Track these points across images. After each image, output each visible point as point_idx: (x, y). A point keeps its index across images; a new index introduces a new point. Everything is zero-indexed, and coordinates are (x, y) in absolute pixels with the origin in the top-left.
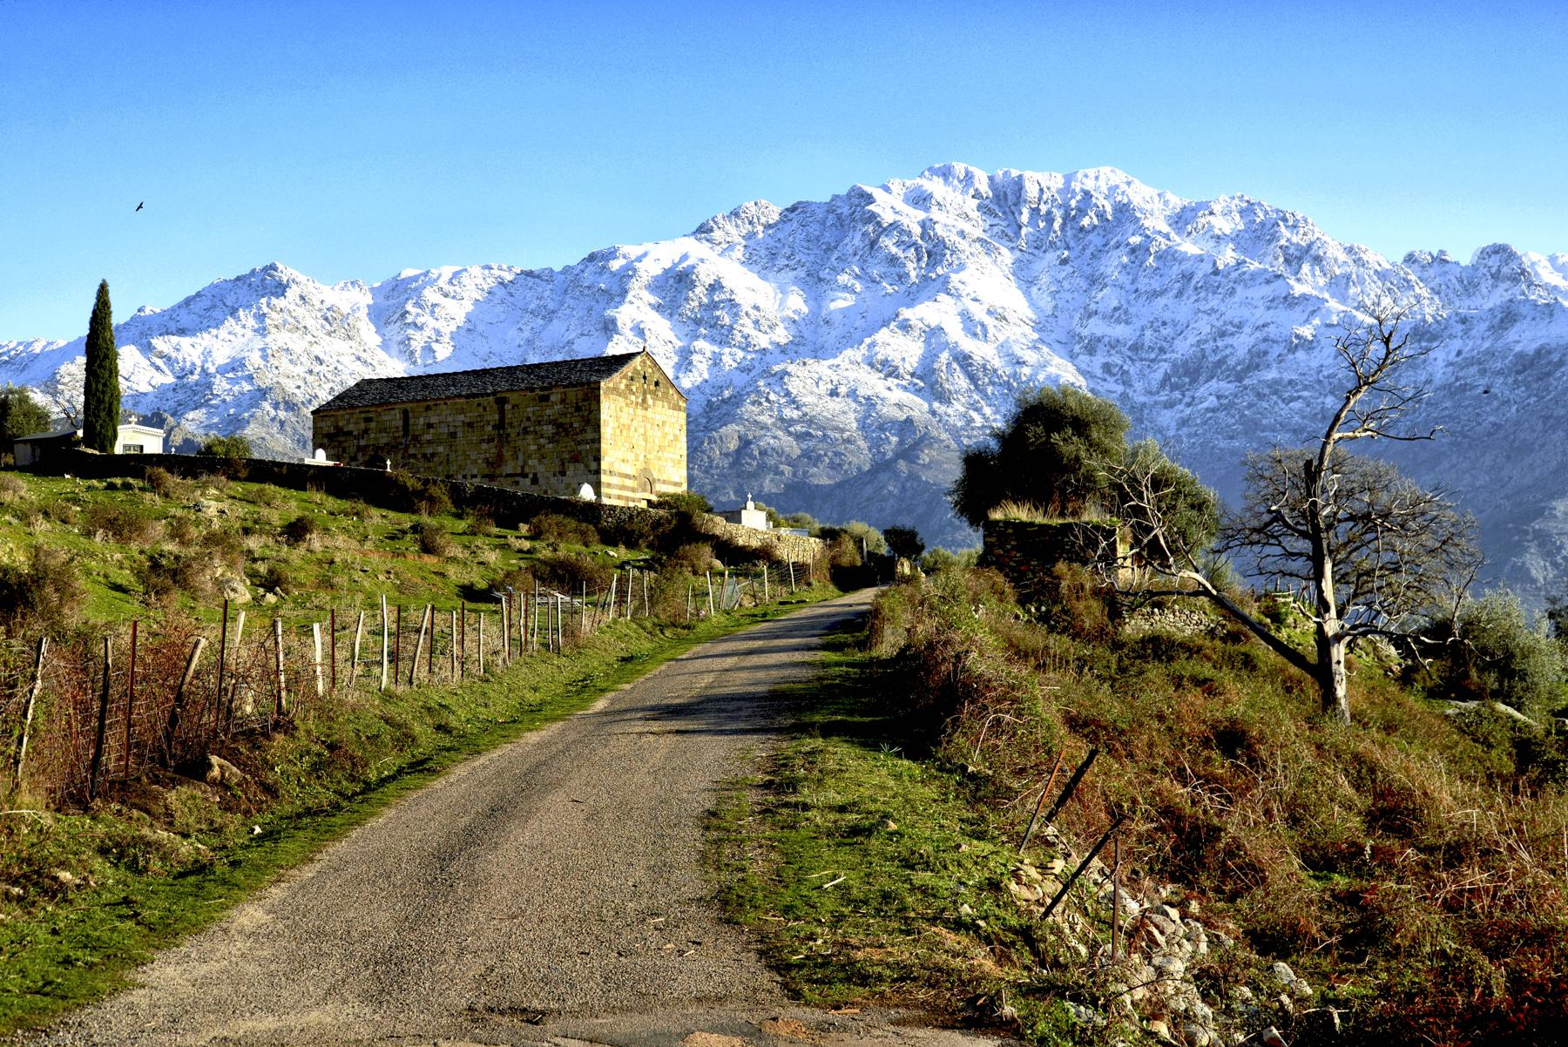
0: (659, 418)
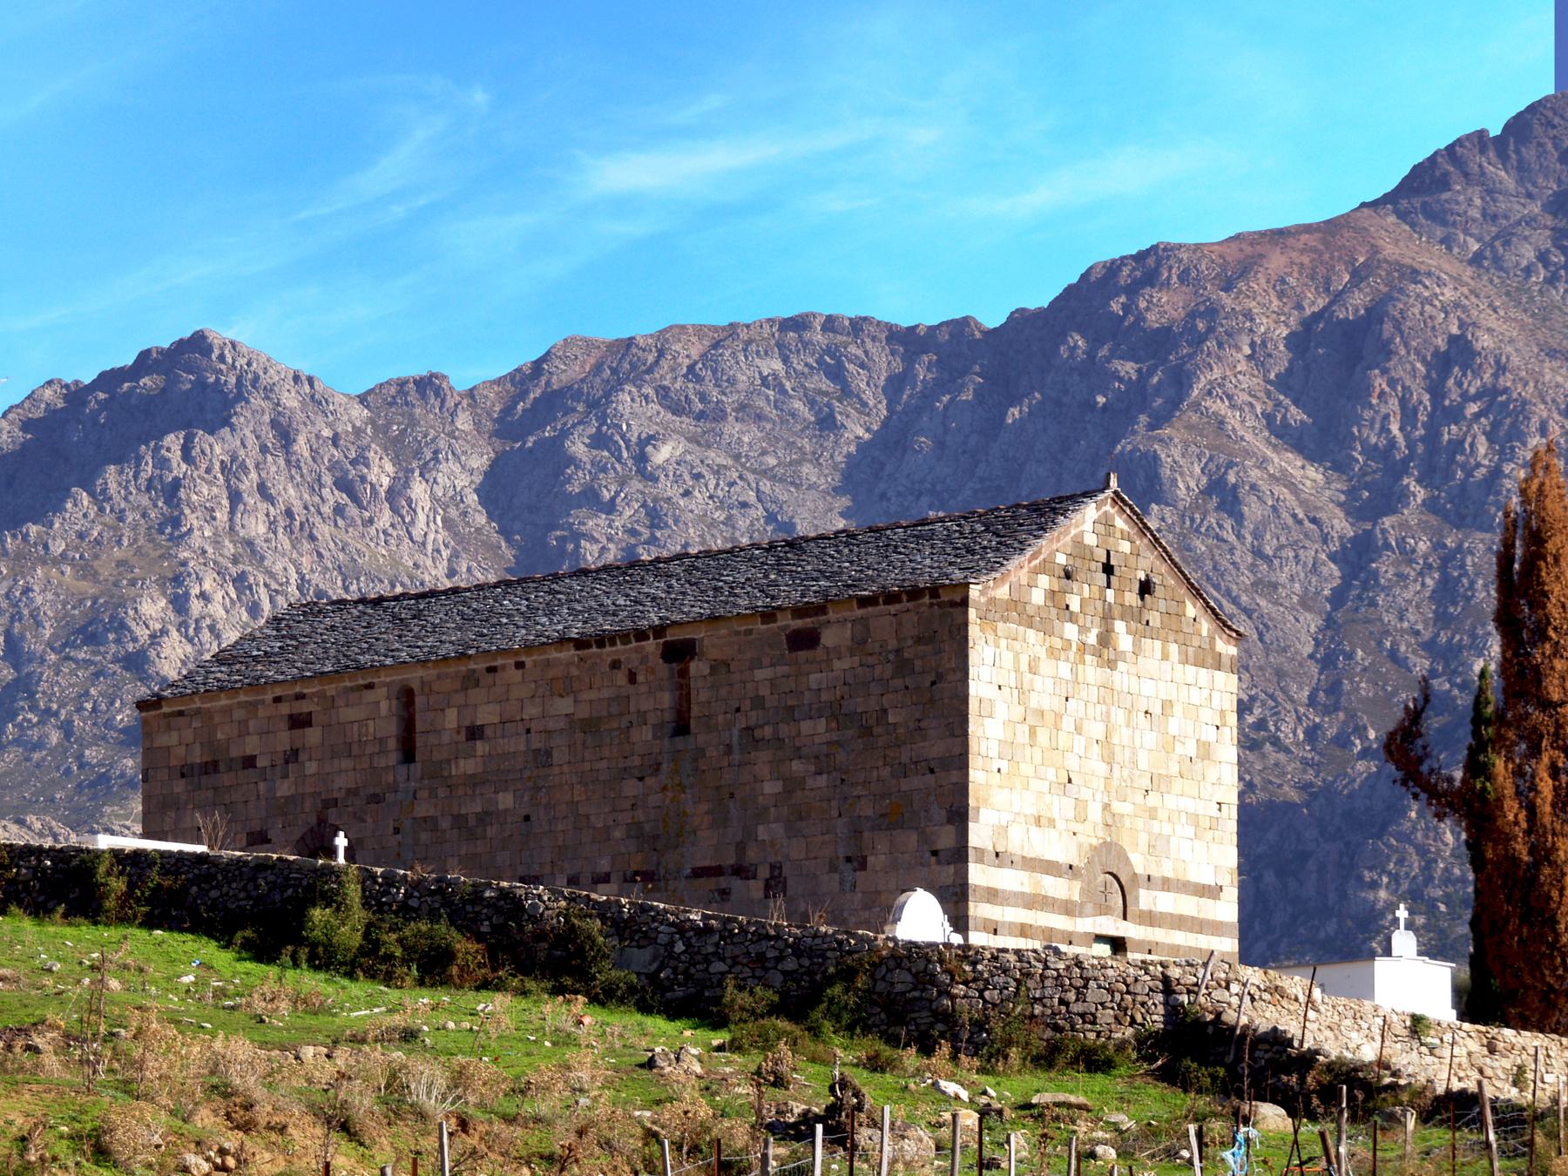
0: (1151, 692)
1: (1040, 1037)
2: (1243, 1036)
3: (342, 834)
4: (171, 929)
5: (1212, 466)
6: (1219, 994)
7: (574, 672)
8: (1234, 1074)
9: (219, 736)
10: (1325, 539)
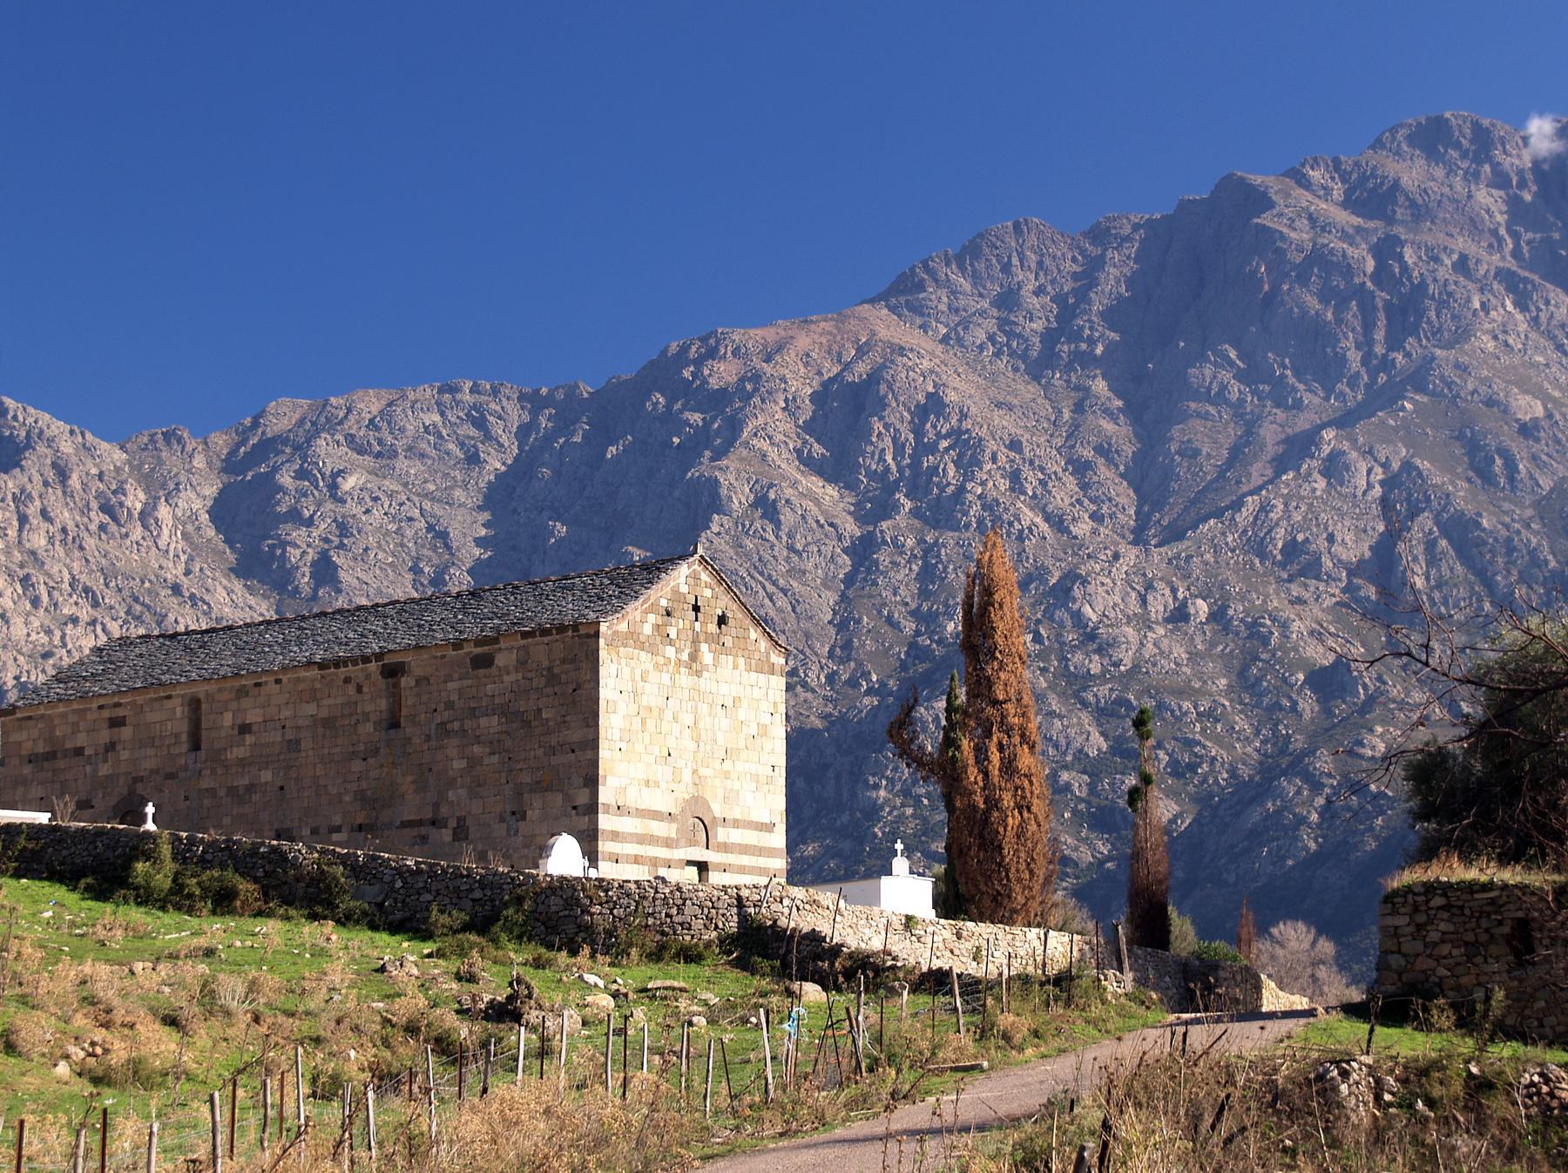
0: (726, 691)
1: (652, 940)
2: (792, 936)
3: (151, 804)
4: (33, 878)
5: (758, 487)
6: (775, 907)
7: (318, 685)
8: (786, 965)
9: (58, 733)
10: (840, 538)
